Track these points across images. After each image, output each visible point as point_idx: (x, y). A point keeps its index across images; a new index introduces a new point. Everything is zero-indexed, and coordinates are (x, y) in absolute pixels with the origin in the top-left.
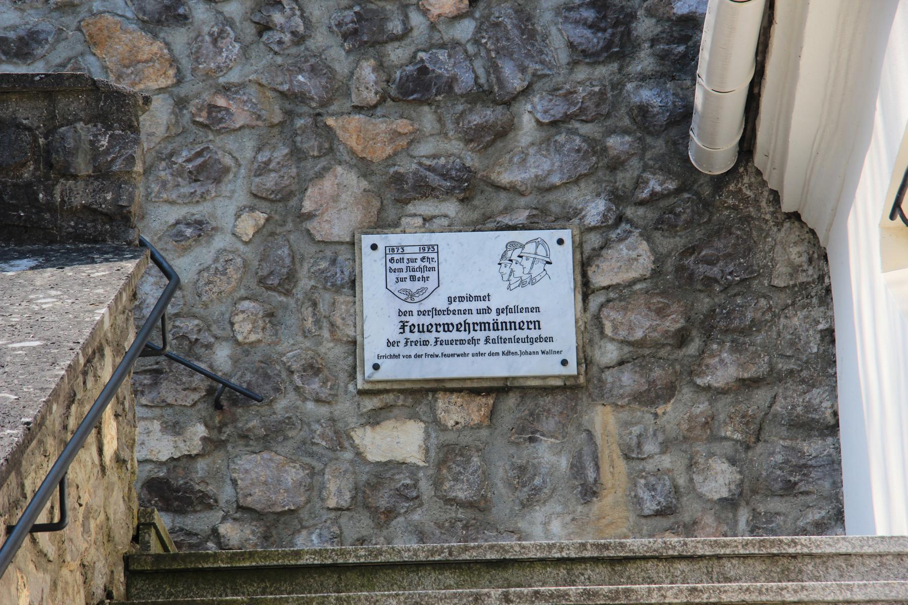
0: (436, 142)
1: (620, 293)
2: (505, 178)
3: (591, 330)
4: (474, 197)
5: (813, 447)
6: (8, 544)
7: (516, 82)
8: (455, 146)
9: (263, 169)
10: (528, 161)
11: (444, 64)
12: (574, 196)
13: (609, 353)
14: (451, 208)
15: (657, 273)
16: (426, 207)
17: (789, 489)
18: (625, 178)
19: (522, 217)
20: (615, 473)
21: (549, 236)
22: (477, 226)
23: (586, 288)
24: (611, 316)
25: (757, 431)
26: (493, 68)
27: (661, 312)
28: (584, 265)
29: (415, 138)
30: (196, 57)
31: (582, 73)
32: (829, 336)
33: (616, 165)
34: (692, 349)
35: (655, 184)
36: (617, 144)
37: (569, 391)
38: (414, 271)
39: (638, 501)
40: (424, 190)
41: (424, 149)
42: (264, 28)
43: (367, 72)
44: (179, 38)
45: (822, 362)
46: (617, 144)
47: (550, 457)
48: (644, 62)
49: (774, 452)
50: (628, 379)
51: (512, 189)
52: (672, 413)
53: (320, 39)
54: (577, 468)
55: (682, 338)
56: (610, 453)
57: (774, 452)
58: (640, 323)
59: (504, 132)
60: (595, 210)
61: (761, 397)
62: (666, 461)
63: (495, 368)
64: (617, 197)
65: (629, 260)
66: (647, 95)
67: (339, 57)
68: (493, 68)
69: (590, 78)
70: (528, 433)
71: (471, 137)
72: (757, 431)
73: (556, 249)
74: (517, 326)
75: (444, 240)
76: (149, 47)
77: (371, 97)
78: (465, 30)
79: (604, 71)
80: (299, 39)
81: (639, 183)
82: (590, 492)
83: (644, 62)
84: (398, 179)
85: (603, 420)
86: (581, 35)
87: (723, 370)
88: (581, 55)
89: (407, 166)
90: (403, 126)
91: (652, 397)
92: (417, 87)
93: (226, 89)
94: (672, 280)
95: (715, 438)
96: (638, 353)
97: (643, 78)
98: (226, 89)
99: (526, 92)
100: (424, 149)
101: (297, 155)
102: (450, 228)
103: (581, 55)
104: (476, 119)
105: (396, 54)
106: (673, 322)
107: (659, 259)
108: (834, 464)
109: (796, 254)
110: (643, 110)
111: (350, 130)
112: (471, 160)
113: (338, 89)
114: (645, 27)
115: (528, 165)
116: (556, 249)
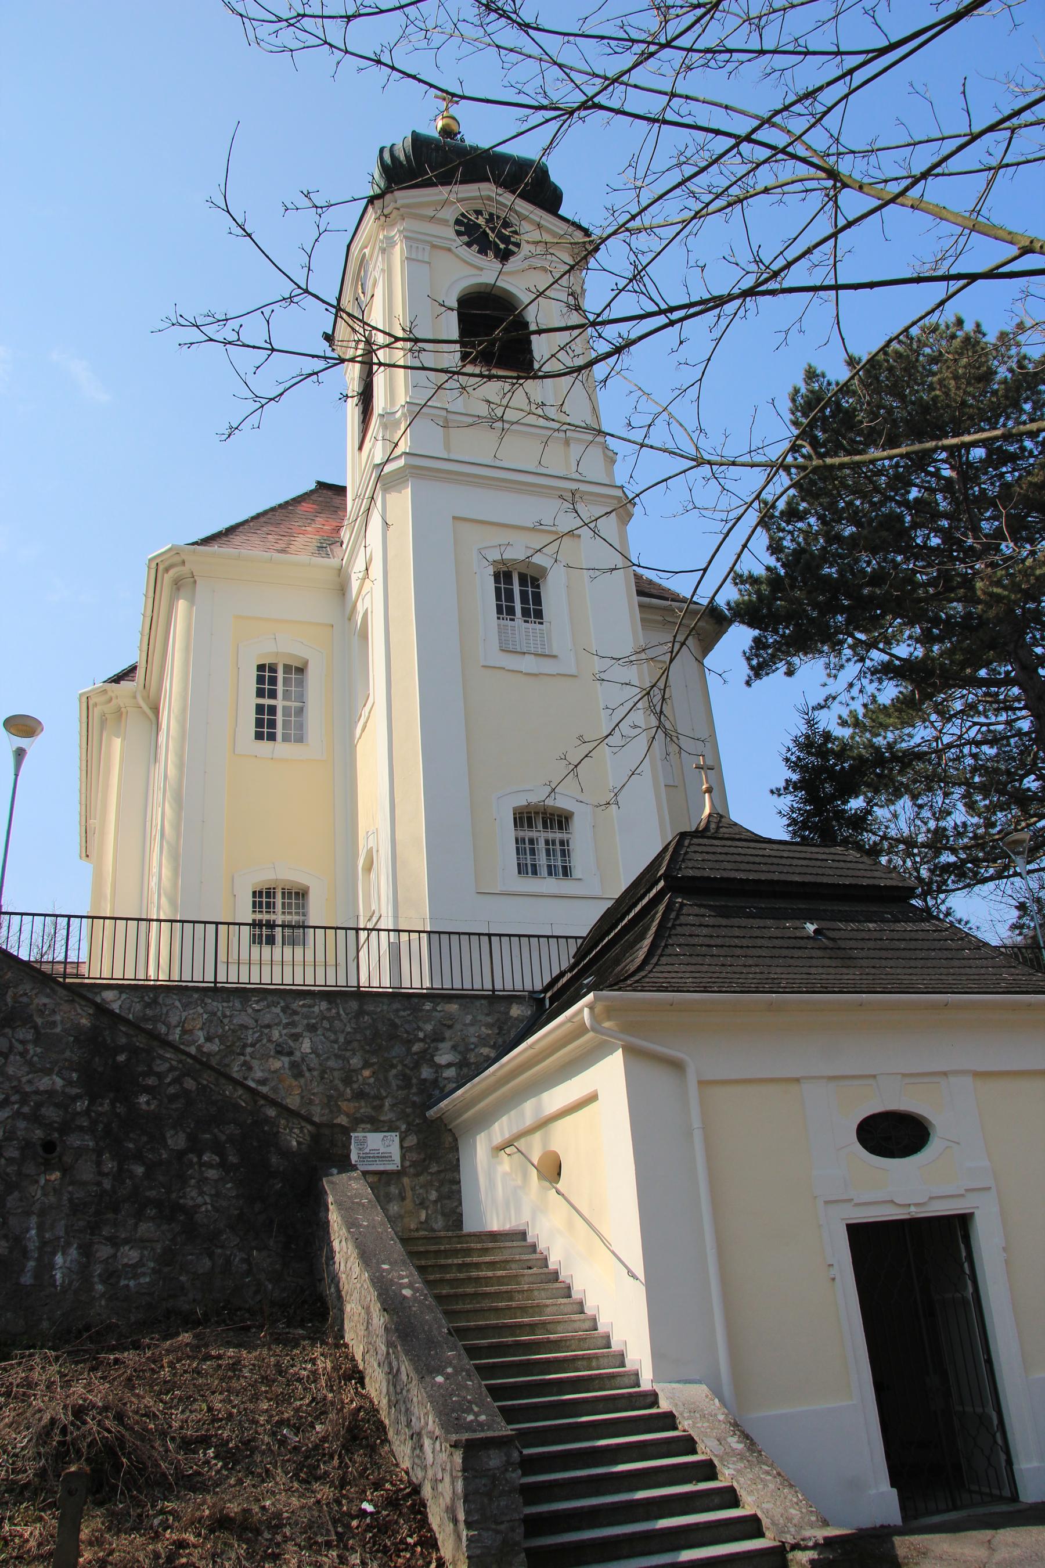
0: (365, 1110)
1: (410, 1149)
2: (382, 1118)
3: (403, 1158)
4: (376, 1125)
5: (454, 1187)
6: (782, 847)
7: (384, 1094)
8: (369, 1110)
9: (323, 1115)
10: (387, 1116)
11: (367, 1089)
12: (398, 1123)
13: (407, 1163)
14: (369, 1126)
15: (418, 1144)
16: (363, 1126)
17: (449, 1198)
18: (410, 1119)
19: (386, 1129)
20: (409, 1194)
21: (394, 1134)
22: (376, 1131)
23: (402, 1147)
24: (408, 1155)
25: (442, 1183)
26: (378, 1090)
27: (419, 1153)
28: (401, 1141)
29: (360, 1107)
30: (306, 1085)
31: (400, 1092)
32: (458, 1160)
33: (408, 1116)
34: (427, 1162)
35: (417, 1121)
36: (408, 1110)
37: (397, 1175)
38: (363, 1142)
39: (414, 1201)
40: (362, 1121)
41: (362, 1111)
42: (322, 1078)
43: (348, 1090)
44: (302, 1081)
45: (456, 1168)
46: (408, 1110)
47: (394, 1190)
48: (414, 1090)
49: (445, 1189)
50: (412, 1170)
51: (384, 1122)
52: (422, 1179)
53: (337, 1082)
54: (400, 1193)
55: (424, 1160)
56: (408, 1189)
57: (445, 1189)
58: (414, 1156)
59: (382, 1106)
60: (404, 1127)
61: (443, 1175)
62: (421, 1191)
63: (381, 1168)
64: (409, 1124)
65: (412, 1140)
66: (415, 1098)
67: (341, 1087)
68: (378, 1090)
69: (401, 1094)
70: (388, 1184)
71: (374, 1108)
72: (442, 1183)
73: (395, 1137)
74: (386, 1158)
75: (367, 1134)
76: (295, 1083)
77: (349, 1097)
78: (372, 1080)
79: (405, 1092)
80: (331, 1081)
81: (414, 1120)
82: (403, 1199)
83: (414, 1090)
84: (356, 1118)
85: (406, 1180)
86: (399, 1082)
87: (434, 1168)
88: (399, 1088)
89: (358, 1115)
90: (357, 1104)
91: (417, 1175)
92: (360, 1095)
93: (313, 1094)
94: (421, 1146)
95: (432, 1185)
96: (414, 1164)
97: (414, 1094)
98: (313, 1094)
99: (386, 1097)
100: (362, 1111)
101: (331, 1112)
102: (369, 1132)
103: (399, 1088)
104: (375, 1103)
105: (355, 1086)
106: (422, 1156)
107: (418, 1140)
108: (460, 1191)
109: (450, 1139)
110: (414, 1103)
111: (344, 1105)
112: (373, 1114)
113: (341, 1095)
114: (414, 1081)
115: (273, 1347)
116: (395, 1137)
